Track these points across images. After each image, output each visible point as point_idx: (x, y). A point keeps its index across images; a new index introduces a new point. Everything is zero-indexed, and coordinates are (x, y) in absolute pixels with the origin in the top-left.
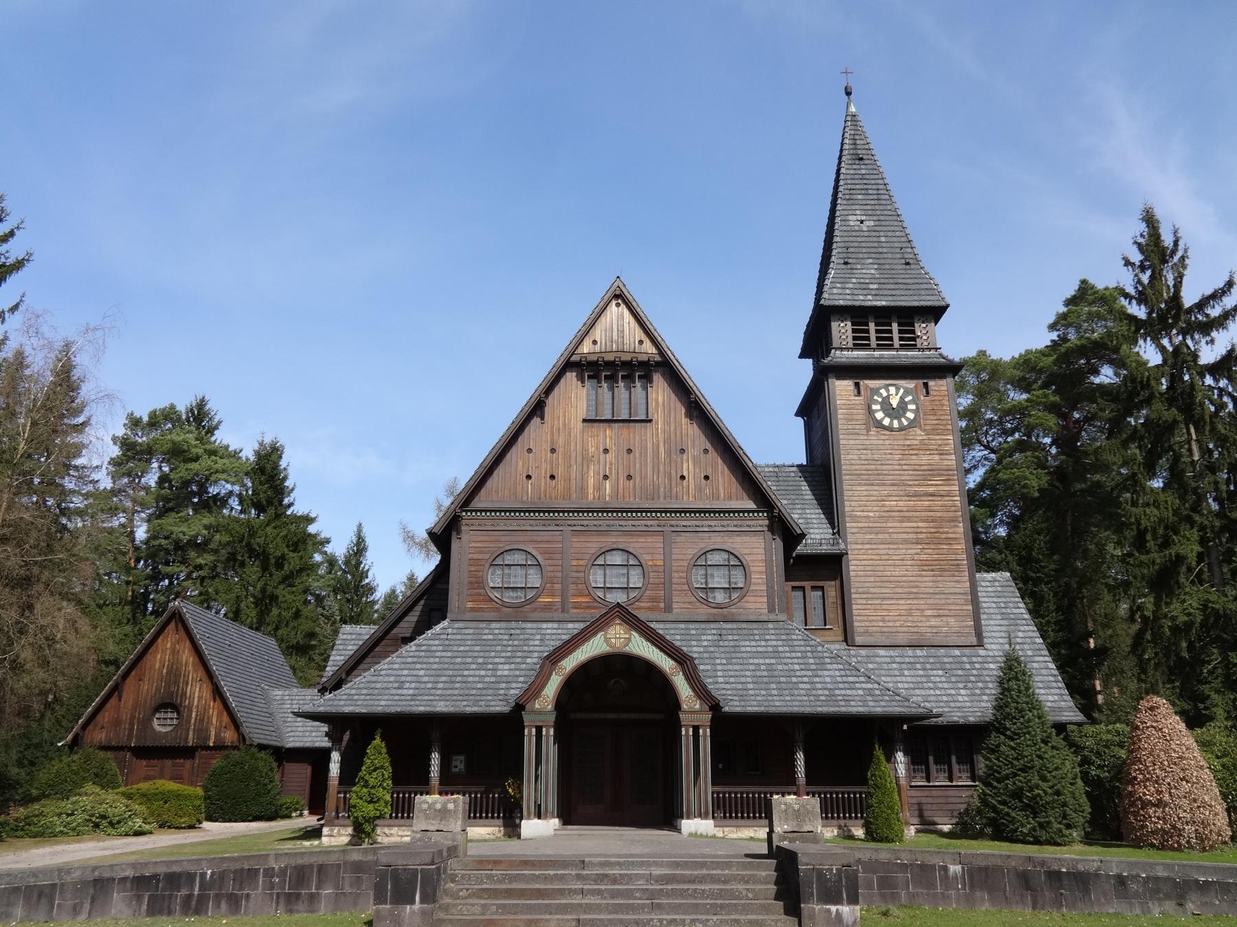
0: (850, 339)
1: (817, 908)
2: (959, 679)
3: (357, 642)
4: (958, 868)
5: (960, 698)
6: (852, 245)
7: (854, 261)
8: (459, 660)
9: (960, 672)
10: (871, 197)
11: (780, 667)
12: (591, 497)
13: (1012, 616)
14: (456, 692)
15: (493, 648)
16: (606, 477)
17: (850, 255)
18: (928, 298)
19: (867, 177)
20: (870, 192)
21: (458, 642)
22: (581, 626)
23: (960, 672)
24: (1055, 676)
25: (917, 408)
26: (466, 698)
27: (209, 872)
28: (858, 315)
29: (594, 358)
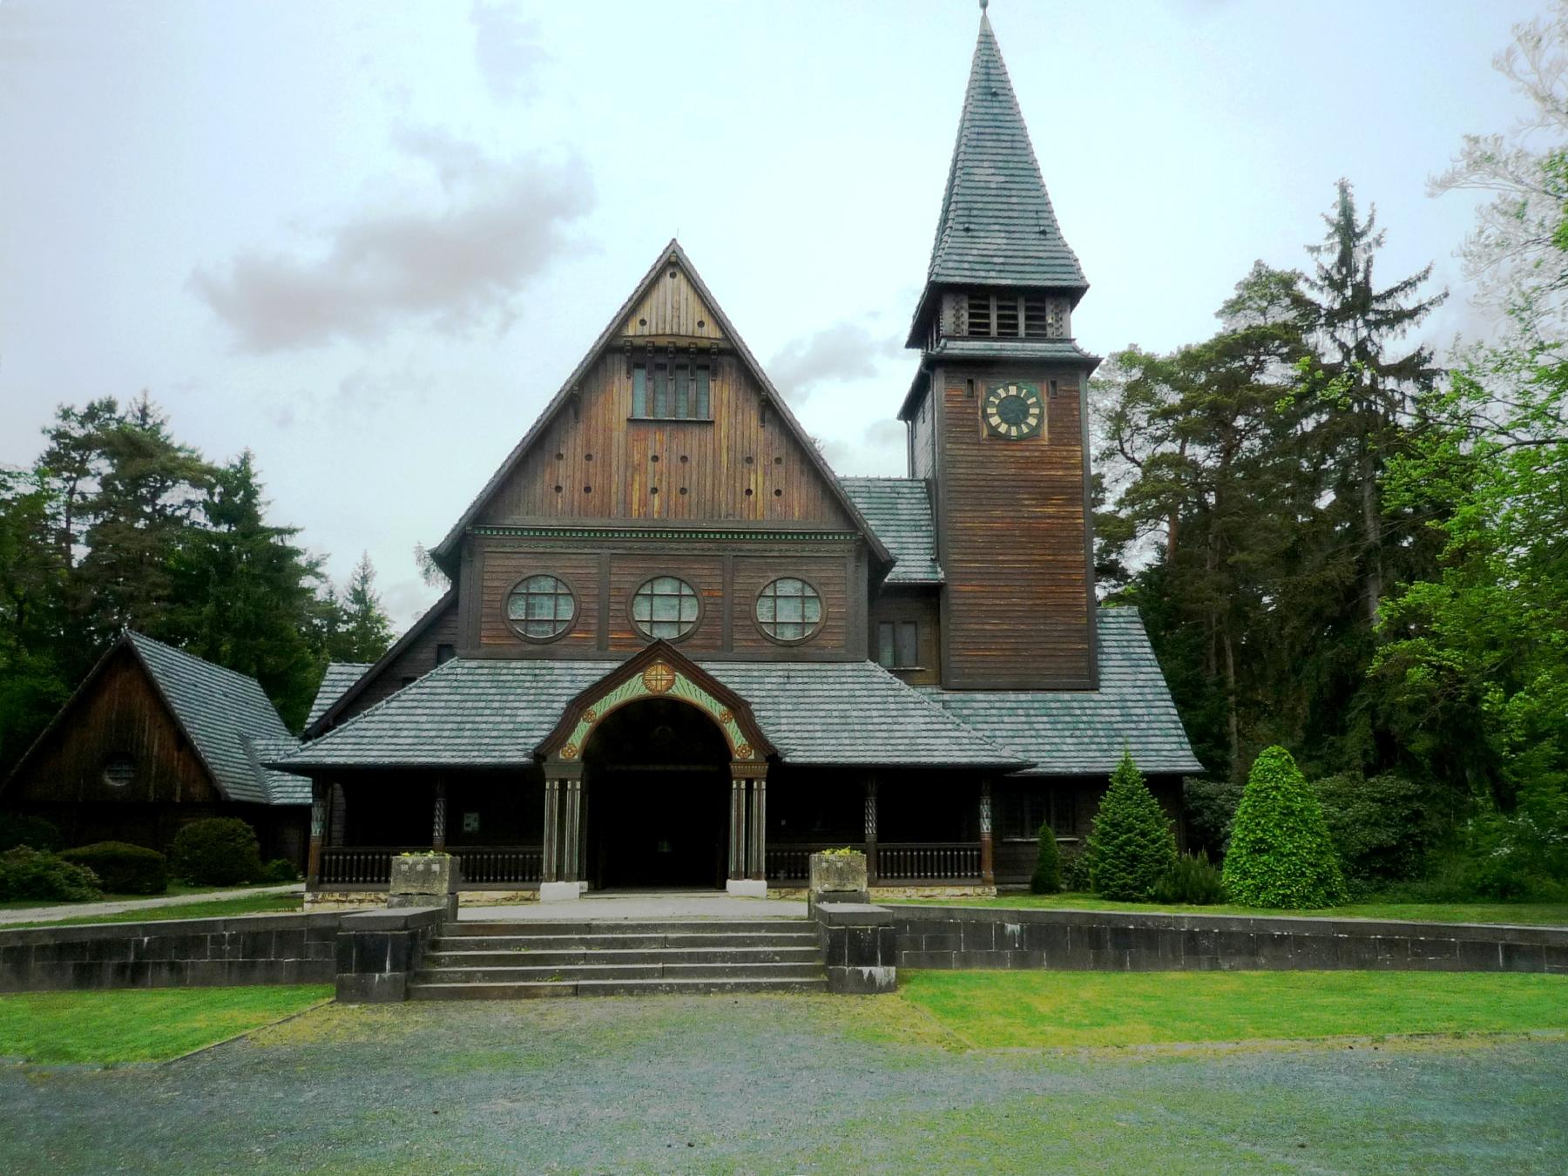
0: (965, 327)
1: (848, 969)
2: (1065, 726)
3: (347, 683)
4: (1017, 928)
5: (1065, 747)
6: (975, 206)
7: (976, 227)
8: (469, 704)
9: (1068, 719)
10: (1004, 145)
11: (855, 713)
12: (635, 514)
13: (1134, 656)
14: (465, 741)
15: (512, 691)
16: (654, 490)
17: (973, 220)
18: (1064, 276)
19: (1001, 118)
20: (1003, 138)
21: (469, 684)
22: (616, 665)
23: (1068, 719)
24: (1175, 722)
25: (1042, 413)
26: (476, 747)
27: (146, 939)
28: (977, 295)
29: (640, 342)
